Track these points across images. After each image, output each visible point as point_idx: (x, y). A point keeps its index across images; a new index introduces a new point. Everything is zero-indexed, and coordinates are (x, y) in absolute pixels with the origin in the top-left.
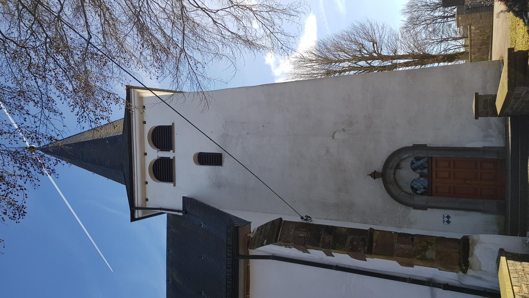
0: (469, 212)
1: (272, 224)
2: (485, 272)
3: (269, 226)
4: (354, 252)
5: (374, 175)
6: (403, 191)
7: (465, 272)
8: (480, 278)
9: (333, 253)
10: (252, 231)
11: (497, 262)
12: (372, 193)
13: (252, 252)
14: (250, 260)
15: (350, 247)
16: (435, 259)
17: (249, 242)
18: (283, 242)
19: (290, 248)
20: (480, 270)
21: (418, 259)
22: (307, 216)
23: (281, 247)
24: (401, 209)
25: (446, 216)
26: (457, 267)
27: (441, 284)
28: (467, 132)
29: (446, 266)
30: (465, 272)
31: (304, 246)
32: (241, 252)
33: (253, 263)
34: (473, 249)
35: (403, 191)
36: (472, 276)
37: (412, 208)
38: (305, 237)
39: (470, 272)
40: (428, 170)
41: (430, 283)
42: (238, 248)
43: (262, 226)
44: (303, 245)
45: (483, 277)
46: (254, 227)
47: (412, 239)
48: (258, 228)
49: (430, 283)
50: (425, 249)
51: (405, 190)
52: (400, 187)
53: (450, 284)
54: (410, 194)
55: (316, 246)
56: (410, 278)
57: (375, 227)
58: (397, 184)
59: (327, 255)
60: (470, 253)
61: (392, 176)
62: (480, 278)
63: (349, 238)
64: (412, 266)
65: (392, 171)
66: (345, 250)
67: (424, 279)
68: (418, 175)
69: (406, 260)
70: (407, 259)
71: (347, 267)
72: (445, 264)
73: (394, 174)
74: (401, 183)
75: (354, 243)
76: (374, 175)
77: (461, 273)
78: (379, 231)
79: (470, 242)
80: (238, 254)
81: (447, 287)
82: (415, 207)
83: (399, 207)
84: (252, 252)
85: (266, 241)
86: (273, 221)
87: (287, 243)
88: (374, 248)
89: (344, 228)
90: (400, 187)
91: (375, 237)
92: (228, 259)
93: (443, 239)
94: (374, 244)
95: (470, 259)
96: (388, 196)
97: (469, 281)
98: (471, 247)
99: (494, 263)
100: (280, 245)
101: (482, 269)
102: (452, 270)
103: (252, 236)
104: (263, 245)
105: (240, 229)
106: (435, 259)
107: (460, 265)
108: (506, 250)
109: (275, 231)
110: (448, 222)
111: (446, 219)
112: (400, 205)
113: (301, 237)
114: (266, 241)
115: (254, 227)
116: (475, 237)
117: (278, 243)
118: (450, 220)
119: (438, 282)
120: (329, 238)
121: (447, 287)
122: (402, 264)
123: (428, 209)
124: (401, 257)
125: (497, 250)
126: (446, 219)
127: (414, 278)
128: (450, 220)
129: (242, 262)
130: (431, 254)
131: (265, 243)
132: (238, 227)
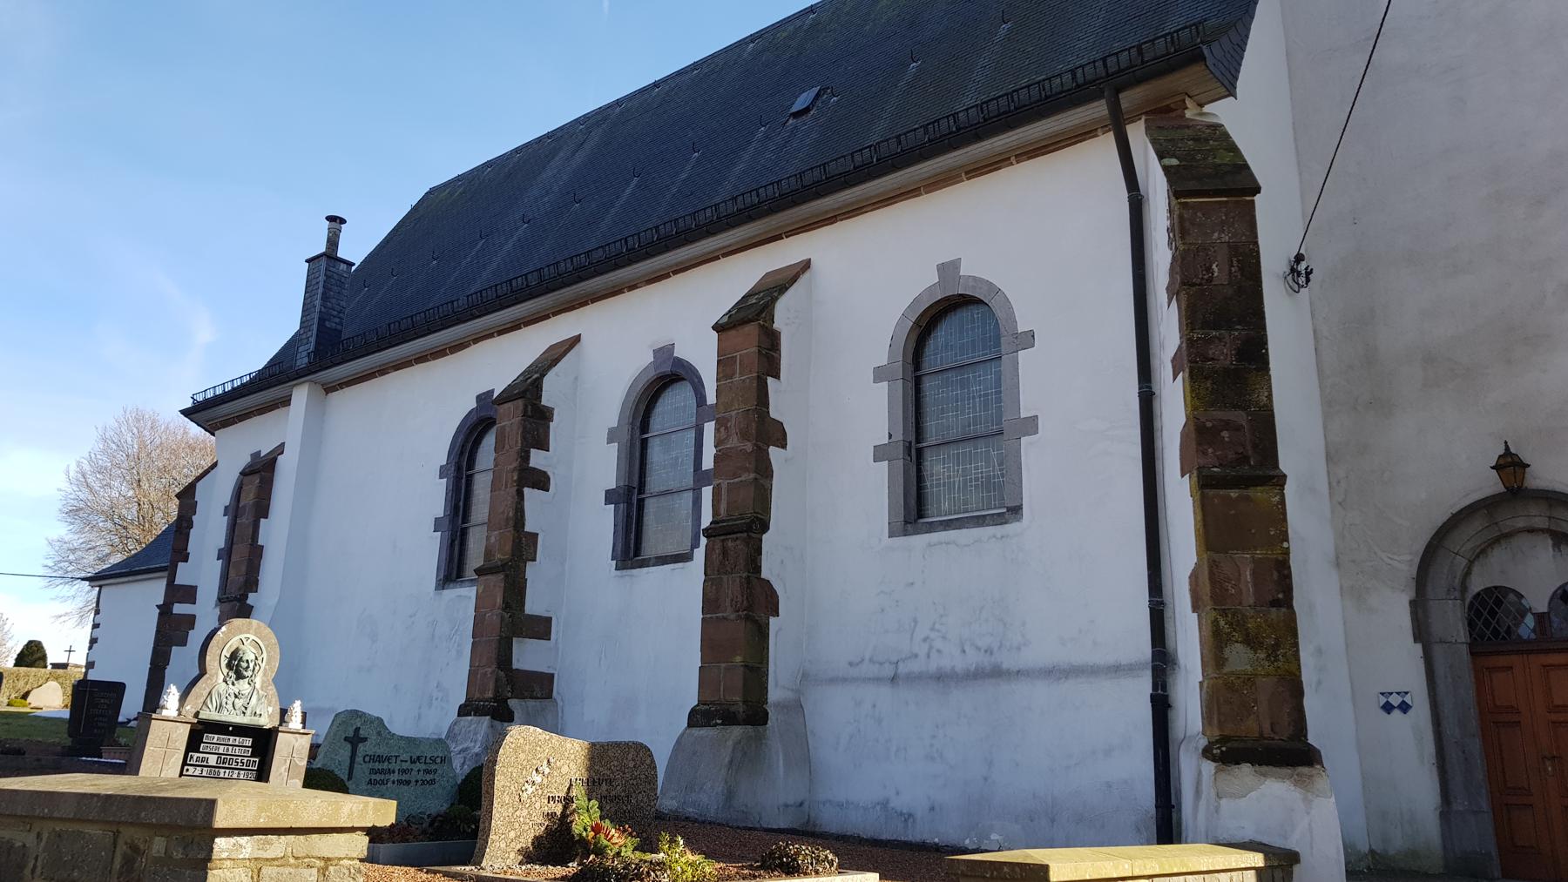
0: (1434, 769)
1: (1235, 165)
2: (1217, 810)
3: (1228, 158)
4: (1199, 434)
5: (1510, 465)
6: (1471, 563)
7: (1207, 753)
8: (1198, 793)
9: (1180, 376)
10: (1207, 108)
11: (1251, 842)
12: (1446, 464)
13: (1137, 134)
14: (1111, 134)
15: (1209, 424)
16: (1226, 670)
17: (1168, 110)
18: (1181, 217)
19: (1170, 244)
20: (1219, 796)
21: (1215, 622)
22: (1308, 273)
23: (1166, 214)
24: (1406, 562)
25: (1408, 699)
26: (1217, 733)
27: (1164, 688)
28: (68, 742)
29: (1219, 699)
30: (1207, 753)
31: (1183, 283)
32: (1128, 99)
33: (1105, 145)
34: (1282, 778)
35: (1471, 563)
36: (1200, 773)
37: (1411, 594)
38: (1210, 280)
39: (1209, 767)
40: (1529, 641)
41: (1162, 660)
42: (1139, 81)
43: (1226, 136)
44: (1187, 282)
45: (1203, 803)
46: (1222, 112)
47: (1276, 603)
48: (1217, 127)
49: (1162, 660)
50: (1251, 642)
51: (1476, 569)
52: (1483, 552)
53: (1172, 714)
54: (1464, 588)
55: (1192, 320)
56: (1162, 603)
57: (1290, 490)
58: (1497, 541)
59: (1173, 361)
60: (1264, 768)
61: (1521, 523)
62: (1198, 793)
63: (1240, 417)
64: (1195, 608)
65: (1540, 522)
66: (1195, 408)
67: (1170, 643)
68: (1542, 607)
69: (1206, 588)
70: (1213, 591)
71: (1157, 424)
72: (1222, 697)
73: (1531, 531)
74: (1498, 556)
75: (1225, 434)
76: (1510, 465)
77: (1203, 742)
78: (1283, 502)
79: (1305, 770)
80: (1118, 91)
81: (1161, 706)
82: (1419, 608)
83: (1409, 557)
84: (1137, 134)
85: (1174, 162)
86: (1246, 167)
87: (1180, 229)
88: (1222, 492)
89: (1270, 396)
90: (1482, 552)
91: (1258, 493)
92: (1099, 64)
93: (1298, 692)
94: (1234, 494)
95: (1246, 768)
96: (1441, 517)
97: (1191, 767)
98: (1287, 771)
99: (1249, 834)
100: (1170, 211)
101: (1223, 802)
102: (1207, 717)
103: (1188, 114)
104: (1161, 157)
105: (1196, 70)
106: (1226, 670)
107: (1223, 740)
108: (1296, 869)
109: (1214, 184)
110: (1388, 708)
111: (1395, 700)
112: (1417, 560)
113: (1209, 269)
114: (1174, 162)
115: (1222, 112)
116: (1322, 783)
117: (1174, 202)
118: (1397, 713)
119: (1170, 681)
120: (1223, 354)
121: (1161, 706)
122: (1194, 577)
123: (1419, 647)
124: (1211, 574)
125: (1292, 844)
126: (1395, 700)
127: (1168, 614)
128: (1397, 713)
129: (1098, 109)
130: (1240, 658)
131: (1167, 161)
132: (1204, 59)
